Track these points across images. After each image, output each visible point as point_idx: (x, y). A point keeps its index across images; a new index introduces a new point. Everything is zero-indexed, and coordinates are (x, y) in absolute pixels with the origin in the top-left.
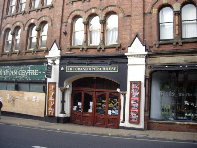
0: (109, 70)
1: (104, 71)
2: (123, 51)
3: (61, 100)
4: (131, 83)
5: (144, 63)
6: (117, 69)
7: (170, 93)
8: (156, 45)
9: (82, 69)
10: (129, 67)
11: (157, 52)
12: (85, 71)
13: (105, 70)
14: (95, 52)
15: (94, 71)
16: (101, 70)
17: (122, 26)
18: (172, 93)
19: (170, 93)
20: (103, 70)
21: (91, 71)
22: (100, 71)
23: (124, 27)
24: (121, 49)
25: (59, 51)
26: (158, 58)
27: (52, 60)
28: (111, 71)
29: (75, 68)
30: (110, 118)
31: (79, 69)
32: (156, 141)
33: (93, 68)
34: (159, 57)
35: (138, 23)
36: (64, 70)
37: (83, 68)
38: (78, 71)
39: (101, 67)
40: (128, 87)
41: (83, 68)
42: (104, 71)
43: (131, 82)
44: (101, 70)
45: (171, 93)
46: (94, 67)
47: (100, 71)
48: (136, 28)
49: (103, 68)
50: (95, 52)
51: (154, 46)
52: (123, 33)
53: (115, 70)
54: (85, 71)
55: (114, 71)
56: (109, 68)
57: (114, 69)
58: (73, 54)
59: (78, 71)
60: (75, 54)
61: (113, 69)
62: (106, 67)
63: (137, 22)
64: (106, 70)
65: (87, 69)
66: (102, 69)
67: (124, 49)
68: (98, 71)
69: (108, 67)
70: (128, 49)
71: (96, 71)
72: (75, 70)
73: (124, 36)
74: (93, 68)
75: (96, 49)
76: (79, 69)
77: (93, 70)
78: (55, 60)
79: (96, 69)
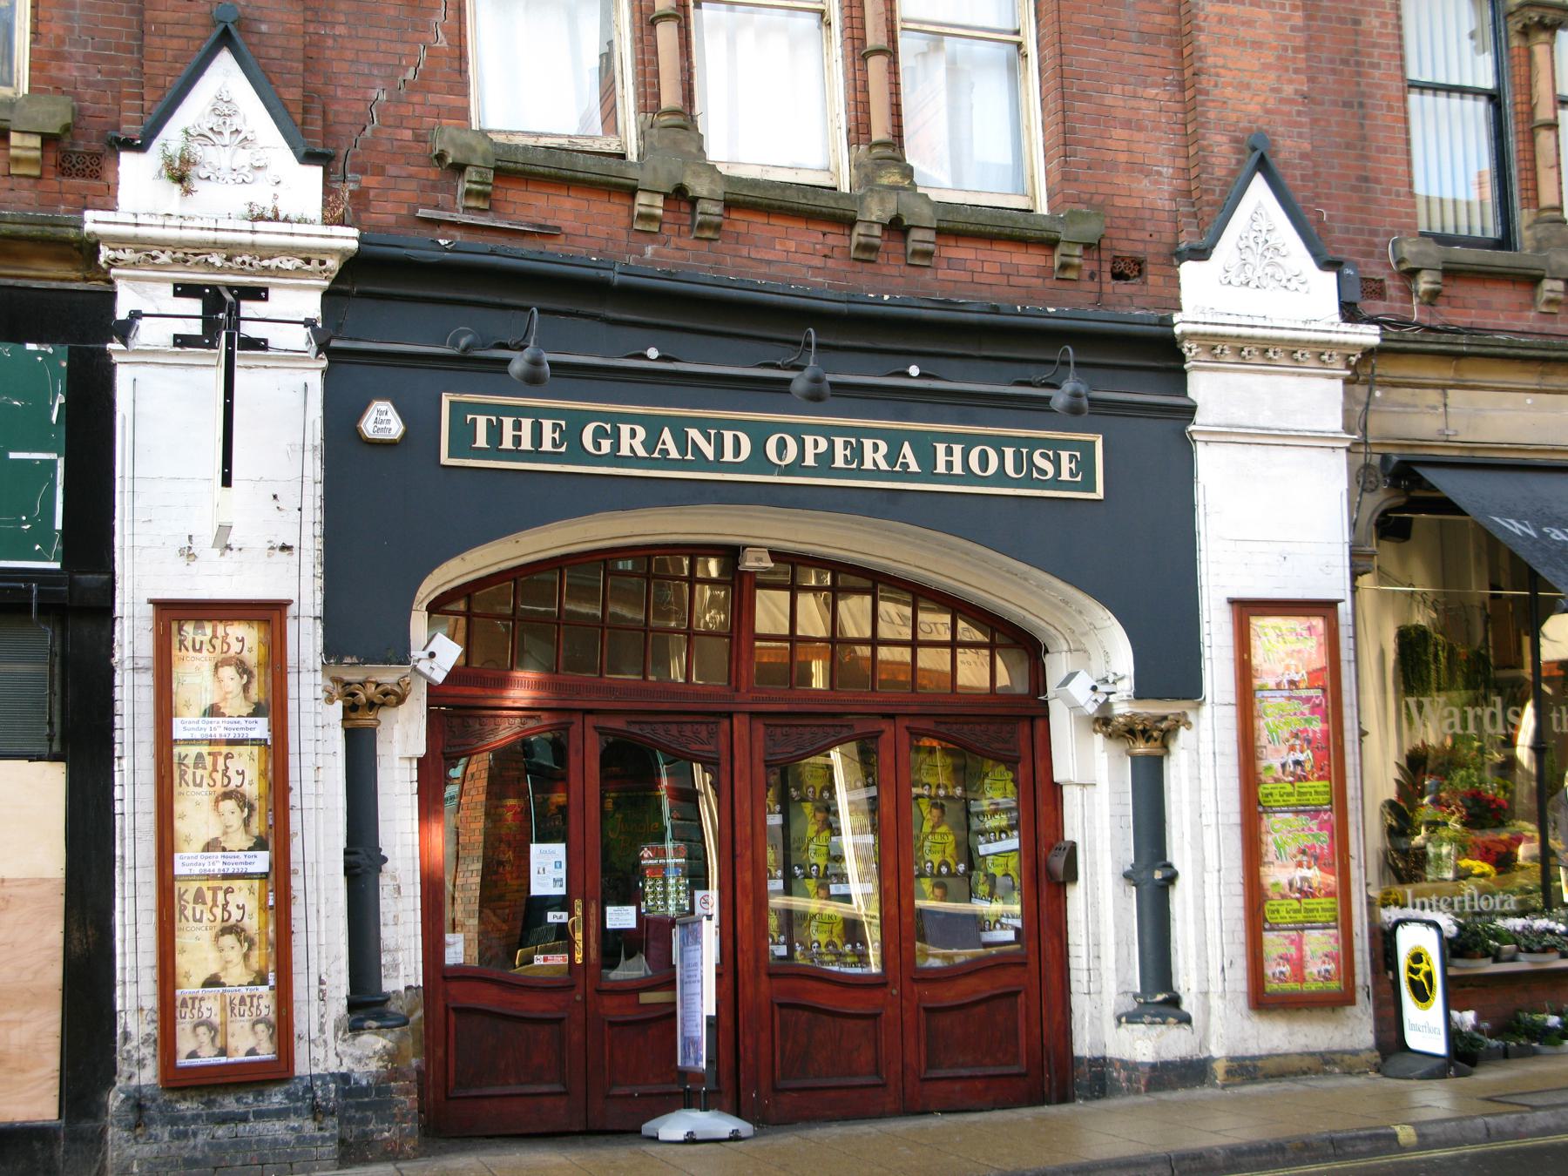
0: (1001, 478)
1: (950, 478)
2: (1122, 287)
3: (1130, 857)
4: (1245, 610)
5: (1332, 419)
6: (1086, 466)
7: (1493, 715)
8: (1412, 274)
9: (681, 441)
10: (1211, 464)
11: (1432, 337)
12: (718, 464)
13: (958, 469)
14: (818, 262)
15: (840, 473)
16: (914, 467)
17: (1095, 31)
18: (1505, 709)
19: (1493, 715)
20: (941, 468)
21: (797, 467)
22: (906, 475)
23: (1112, 44)
24: (1107, 267)
25: (316, 173)
26: (1433, 396)
27: (184, 290)
28: (1029, 482)
29: (576, 422)
30: (949, 995)
31: (632, 441)
32: (1362, 1163)
33: (814, 447)
34: (1444, 388)
35: (1259, 32)
36: (405, 436)
37: (694, 433)
38: (614, 458)
39: (914, 437)
40: (1206, 653)
41: (694, 433)
42: (950, 478)
43: (1233, 602)
44: (914, 467)
45: (1498, 710)
46: (829, 432)
47: (906, 475)
48: (1248, 86)
49: (941, 448)
50: (818, 262)
51: (1392, 286)
52: (1109, 100)
53: (1065, 476)
54: (718, 464)
55: (1056, 483)
56: (1009, 452)
57: (1057, 463)
58: (527, 246)
59: (614, 458)
60: (550, 246)
61: (1049, 468)
62: (969, 442)
63: (1249, 23)
64: (968, 477)
65: (588, 431)
66: (926, 457)
67: (1128, 269)
68: (876, 474)
69: (998, 443)
70: (1175, 282)
71: (861, 473)
72: (766, 466)
73: (1118, 133)
74: (814, 447)
75: (847, 222)
76: (632, 441)
77: (826, 459)
78: (258, 294)
79: (858, 453)
